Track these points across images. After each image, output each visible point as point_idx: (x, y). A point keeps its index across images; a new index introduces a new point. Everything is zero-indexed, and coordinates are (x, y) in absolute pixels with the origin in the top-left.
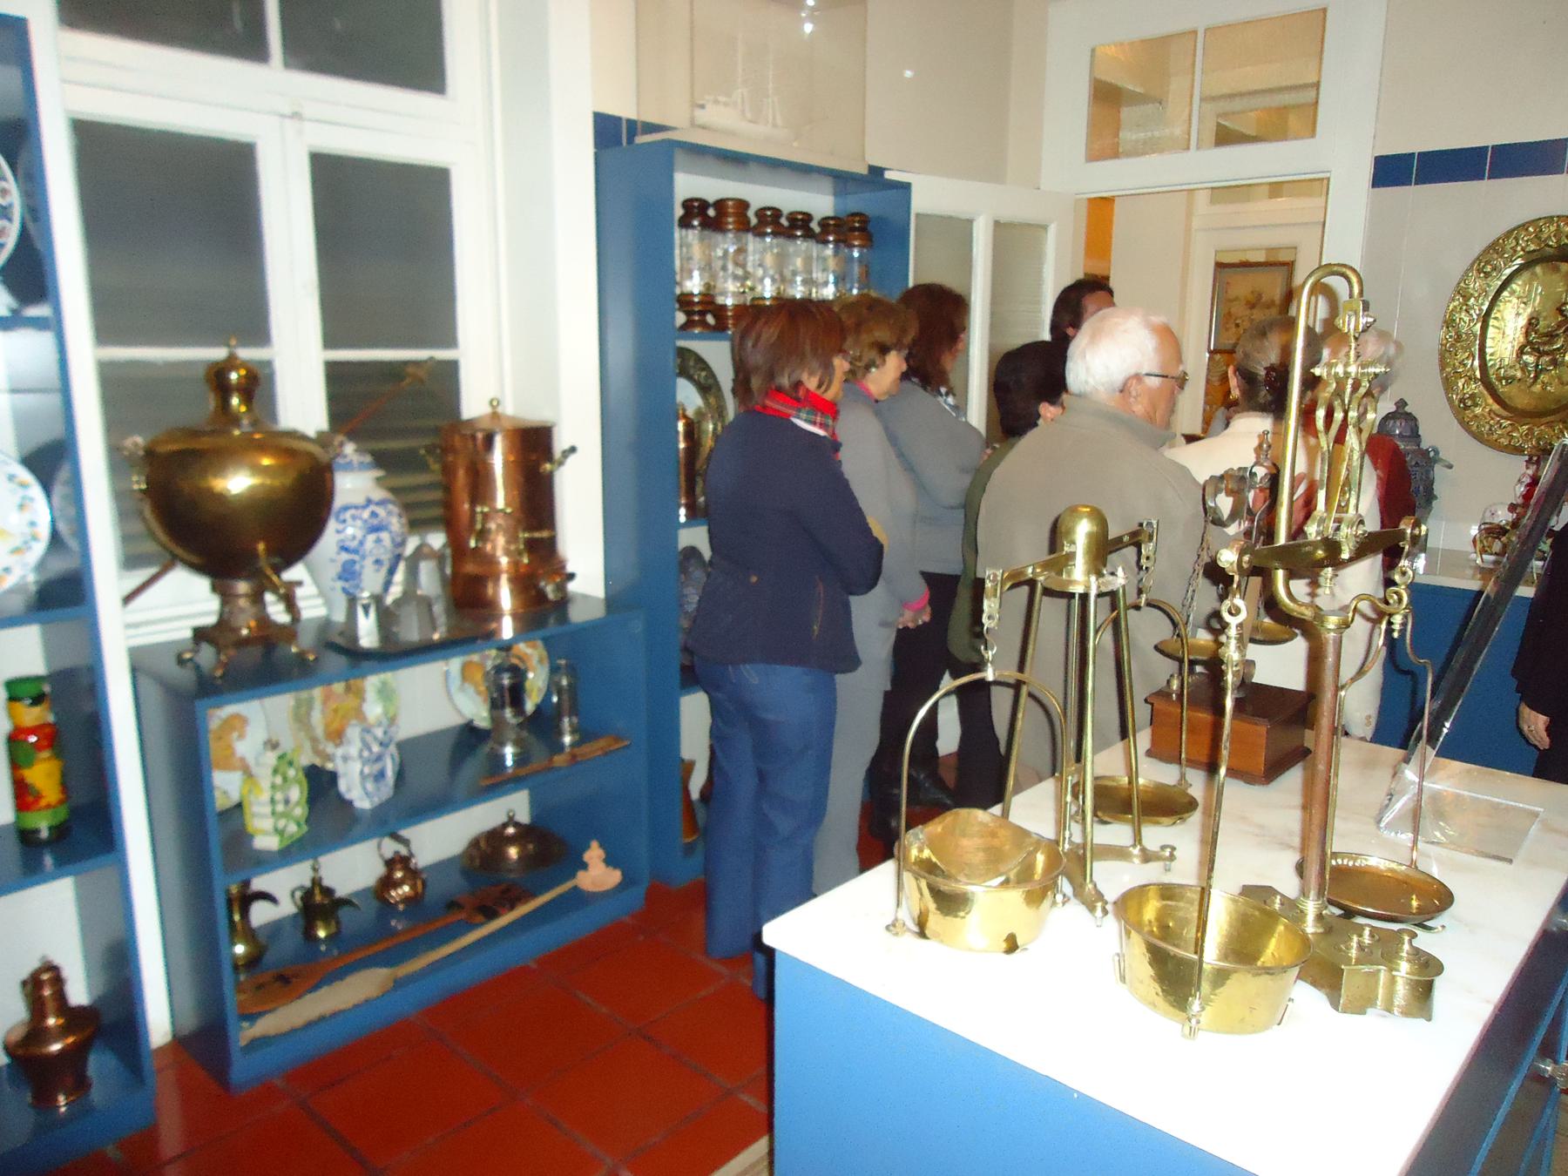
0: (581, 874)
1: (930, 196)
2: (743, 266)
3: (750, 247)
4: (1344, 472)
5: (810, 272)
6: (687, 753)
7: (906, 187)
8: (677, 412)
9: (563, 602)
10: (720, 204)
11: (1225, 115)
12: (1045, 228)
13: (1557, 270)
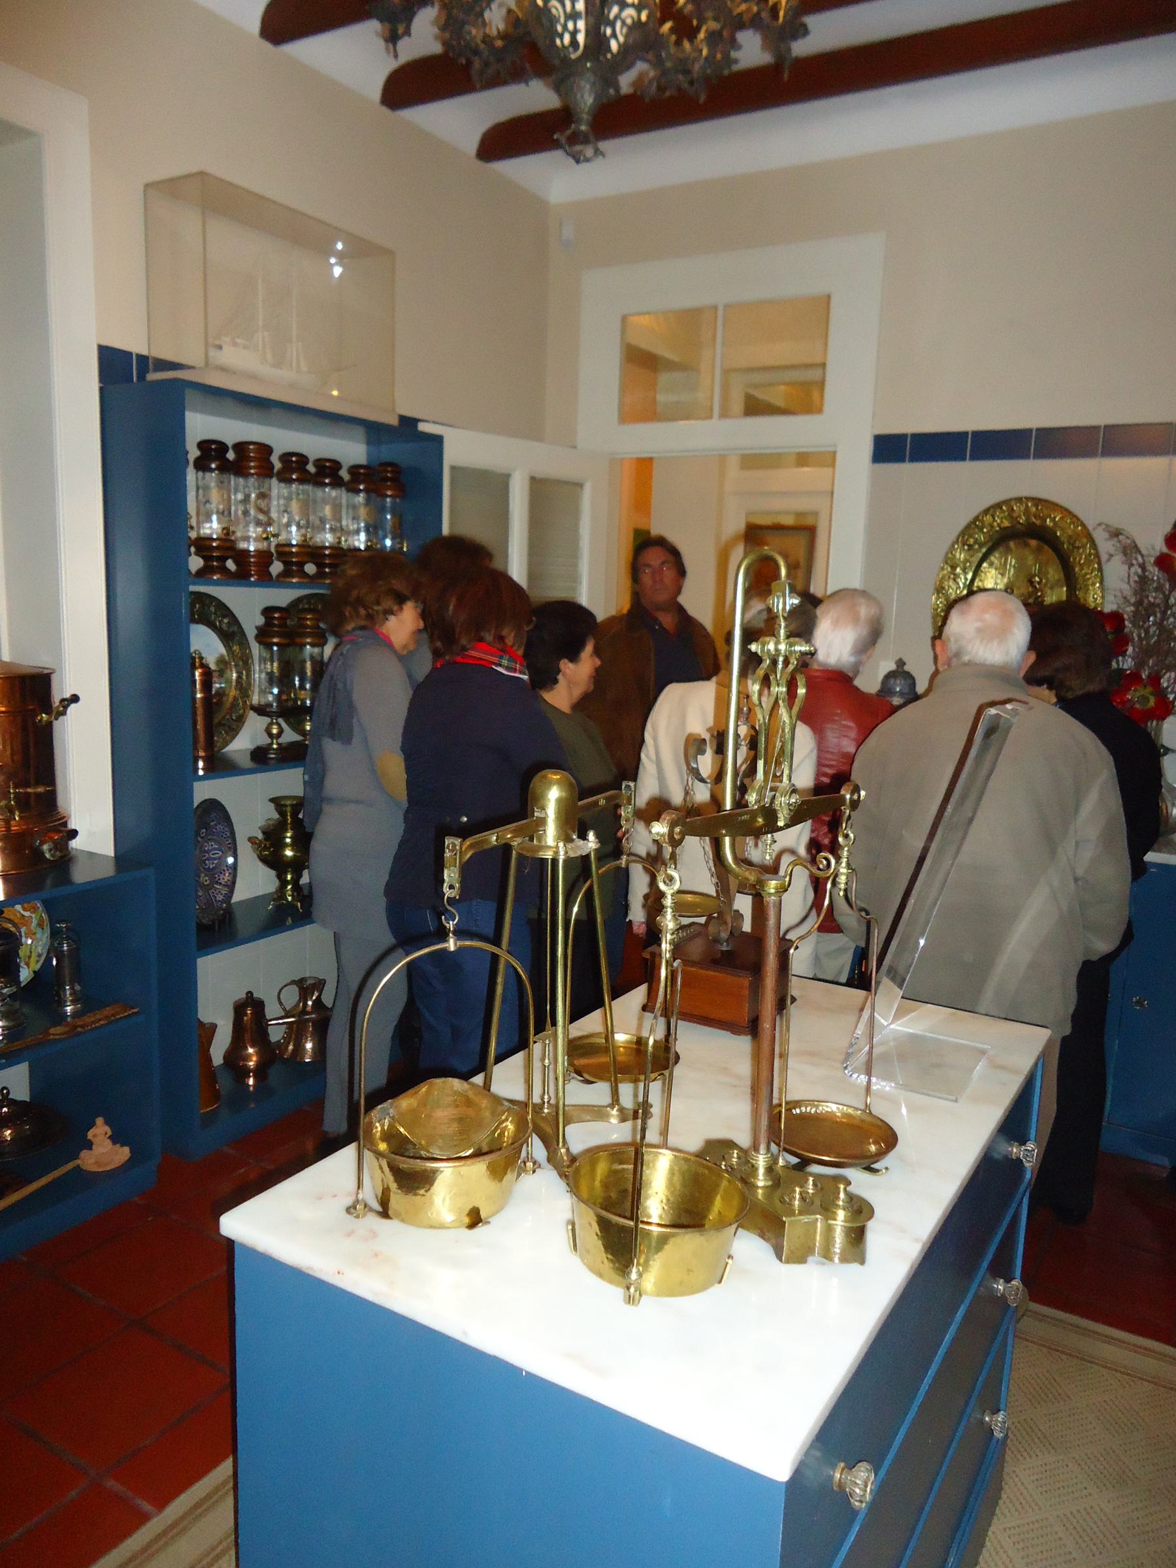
0: (84, 1154)
1: (462, 449)
2: (266, 512)
3: (274, 492)
4: (778, 744)
5: (340, 521)
6: (205, 1014)
7: (438, 440)
8: (195, 661)
9: (65, 860)
10: (240, 447)
11: (756, 386)
12: (580, 485)
13: (1026, 545)
